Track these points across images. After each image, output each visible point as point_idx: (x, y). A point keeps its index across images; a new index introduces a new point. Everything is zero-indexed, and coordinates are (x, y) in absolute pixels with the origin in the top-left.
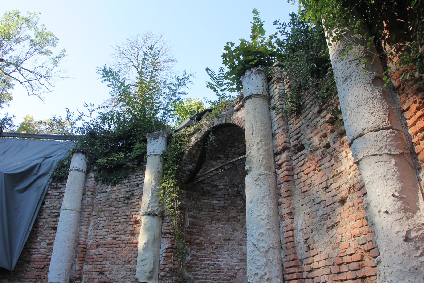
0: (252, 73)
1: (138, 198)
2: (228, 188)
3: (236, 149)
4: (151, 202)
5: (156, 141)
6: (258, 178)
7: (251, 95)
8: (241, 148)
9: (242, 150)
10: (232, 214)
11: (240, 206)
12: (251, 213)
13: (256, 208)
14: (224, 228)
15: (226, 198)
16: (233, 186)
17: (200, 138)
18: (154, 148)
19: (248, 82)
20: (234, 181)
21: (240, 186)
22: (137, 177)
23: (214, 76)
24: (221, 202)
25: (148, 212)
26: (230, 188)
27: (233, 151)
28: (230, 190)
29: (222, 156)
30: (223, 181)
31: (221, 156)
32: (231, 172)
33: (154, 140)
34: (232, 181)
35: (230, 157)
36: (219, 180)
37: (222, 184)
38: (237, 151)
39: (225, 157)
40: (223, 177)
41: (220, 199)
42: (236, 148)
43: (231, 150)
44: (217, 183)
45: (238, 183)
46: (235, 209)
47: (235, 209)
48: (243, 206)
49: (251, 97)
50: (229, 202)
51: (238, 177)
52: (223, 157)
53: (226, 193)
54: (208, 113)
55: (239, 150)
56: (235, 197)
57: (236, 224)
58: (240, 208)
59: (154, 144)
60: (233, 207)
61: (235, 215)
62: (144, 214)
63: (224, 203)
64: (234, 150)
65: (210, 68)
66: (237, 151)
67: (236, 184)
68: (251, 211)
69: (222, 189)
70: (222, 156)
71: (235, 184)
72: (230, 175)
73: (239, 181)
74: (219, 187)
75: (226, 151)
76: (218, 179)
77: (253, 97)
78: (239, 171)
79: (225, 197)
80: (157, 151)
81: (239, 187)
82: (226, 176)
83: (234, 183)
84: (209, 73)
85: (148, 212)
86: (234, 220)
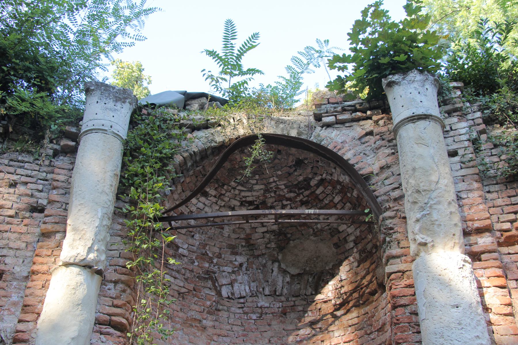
0: (427, 79)
1: (10, 216)
2: (194, 258)
3: (243, 191)
4: (98, 237)
5: (119, 104)
6: (463, 265)
7: (431, 116)
8: (254, 191)
9: (253, 196)
10: (193, 313)
11: (210, 300)
12: (460, 327)
13: (468, 321)
14: (177, 338)
15: (186, 277)
16: (204, 256)
17: (219, 142)
18: (113, 119)
19: (419, 90)
20: (207, 248)
21: (215, 261)
22: (12, 163)
23: (232, 41)
24: (178, 281)
25: (88, 259)
26: (196, 259)
27: (237, 192)
28: (196, 264)
29: (212, 192)
30: (191, 241)
31: (210, 192)
32: (211, 229)
33: (116, 101)
34: (204, 246)
35: (224, 201)
36: (185, 237)
37: (186, 246)
38: (243, 194)
39: (215, 197)
40: (193, 234)
41: (177, 275)
42: (245, 187)
43: (234, 188)
44: (180, 241)
45: (214, 253)
46: (199, 303)
47: (199, 303)
48: (214, 301)
49: (428, 118)
50: (191, 286)
51: (217, 243)
52: (211, 196)
53: (188, 267)
54: (204, 100)
55: (249, 194)
56: (200, 279)
57: (198, 334)
58: (208, 303)
59: (115, 110)
60: (196, 299)
61: (198, 316)
62: (77, 261)
63: (182, 284)
64: (239, 190)
65: (235, 22)
66: (243, 194)
67: (210, 255)
68: (459, 324)
69: (184, 256)
70: (212, 192)
71: (207, 254)
72: (206, 234)
73: (217, 250)
74: (181, 250)
75: (225, 187)
76: (184, 234)
77: (432, 119)
78: (224, 232)
79: (184, 275)
80: (118, 128)
81: (212, 262)
82: (199, 233)
83: (206, 252)
84: (227, 30)
85: (88, 259)
86: (196, 326)
